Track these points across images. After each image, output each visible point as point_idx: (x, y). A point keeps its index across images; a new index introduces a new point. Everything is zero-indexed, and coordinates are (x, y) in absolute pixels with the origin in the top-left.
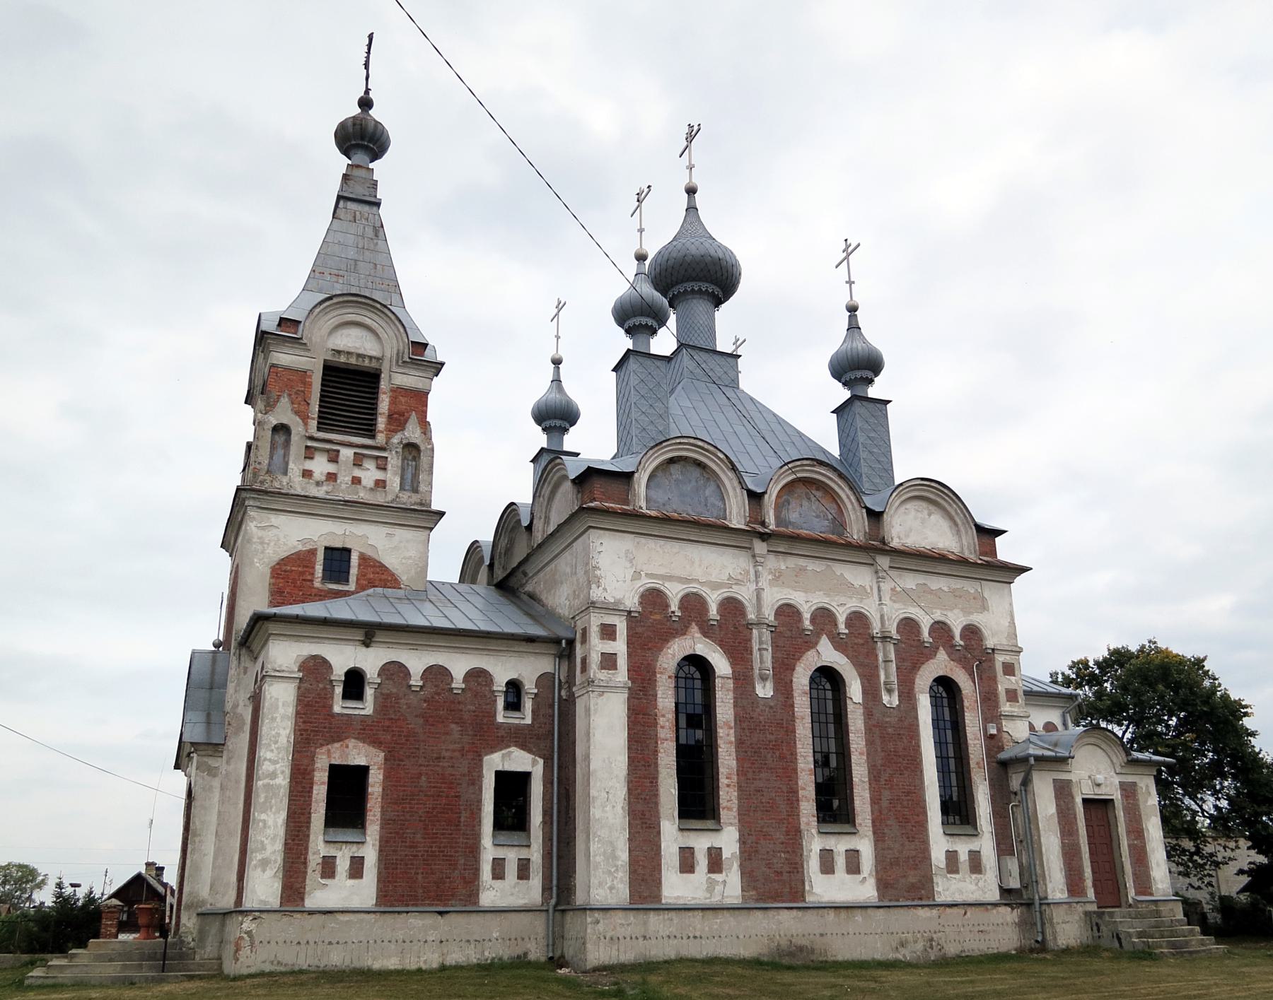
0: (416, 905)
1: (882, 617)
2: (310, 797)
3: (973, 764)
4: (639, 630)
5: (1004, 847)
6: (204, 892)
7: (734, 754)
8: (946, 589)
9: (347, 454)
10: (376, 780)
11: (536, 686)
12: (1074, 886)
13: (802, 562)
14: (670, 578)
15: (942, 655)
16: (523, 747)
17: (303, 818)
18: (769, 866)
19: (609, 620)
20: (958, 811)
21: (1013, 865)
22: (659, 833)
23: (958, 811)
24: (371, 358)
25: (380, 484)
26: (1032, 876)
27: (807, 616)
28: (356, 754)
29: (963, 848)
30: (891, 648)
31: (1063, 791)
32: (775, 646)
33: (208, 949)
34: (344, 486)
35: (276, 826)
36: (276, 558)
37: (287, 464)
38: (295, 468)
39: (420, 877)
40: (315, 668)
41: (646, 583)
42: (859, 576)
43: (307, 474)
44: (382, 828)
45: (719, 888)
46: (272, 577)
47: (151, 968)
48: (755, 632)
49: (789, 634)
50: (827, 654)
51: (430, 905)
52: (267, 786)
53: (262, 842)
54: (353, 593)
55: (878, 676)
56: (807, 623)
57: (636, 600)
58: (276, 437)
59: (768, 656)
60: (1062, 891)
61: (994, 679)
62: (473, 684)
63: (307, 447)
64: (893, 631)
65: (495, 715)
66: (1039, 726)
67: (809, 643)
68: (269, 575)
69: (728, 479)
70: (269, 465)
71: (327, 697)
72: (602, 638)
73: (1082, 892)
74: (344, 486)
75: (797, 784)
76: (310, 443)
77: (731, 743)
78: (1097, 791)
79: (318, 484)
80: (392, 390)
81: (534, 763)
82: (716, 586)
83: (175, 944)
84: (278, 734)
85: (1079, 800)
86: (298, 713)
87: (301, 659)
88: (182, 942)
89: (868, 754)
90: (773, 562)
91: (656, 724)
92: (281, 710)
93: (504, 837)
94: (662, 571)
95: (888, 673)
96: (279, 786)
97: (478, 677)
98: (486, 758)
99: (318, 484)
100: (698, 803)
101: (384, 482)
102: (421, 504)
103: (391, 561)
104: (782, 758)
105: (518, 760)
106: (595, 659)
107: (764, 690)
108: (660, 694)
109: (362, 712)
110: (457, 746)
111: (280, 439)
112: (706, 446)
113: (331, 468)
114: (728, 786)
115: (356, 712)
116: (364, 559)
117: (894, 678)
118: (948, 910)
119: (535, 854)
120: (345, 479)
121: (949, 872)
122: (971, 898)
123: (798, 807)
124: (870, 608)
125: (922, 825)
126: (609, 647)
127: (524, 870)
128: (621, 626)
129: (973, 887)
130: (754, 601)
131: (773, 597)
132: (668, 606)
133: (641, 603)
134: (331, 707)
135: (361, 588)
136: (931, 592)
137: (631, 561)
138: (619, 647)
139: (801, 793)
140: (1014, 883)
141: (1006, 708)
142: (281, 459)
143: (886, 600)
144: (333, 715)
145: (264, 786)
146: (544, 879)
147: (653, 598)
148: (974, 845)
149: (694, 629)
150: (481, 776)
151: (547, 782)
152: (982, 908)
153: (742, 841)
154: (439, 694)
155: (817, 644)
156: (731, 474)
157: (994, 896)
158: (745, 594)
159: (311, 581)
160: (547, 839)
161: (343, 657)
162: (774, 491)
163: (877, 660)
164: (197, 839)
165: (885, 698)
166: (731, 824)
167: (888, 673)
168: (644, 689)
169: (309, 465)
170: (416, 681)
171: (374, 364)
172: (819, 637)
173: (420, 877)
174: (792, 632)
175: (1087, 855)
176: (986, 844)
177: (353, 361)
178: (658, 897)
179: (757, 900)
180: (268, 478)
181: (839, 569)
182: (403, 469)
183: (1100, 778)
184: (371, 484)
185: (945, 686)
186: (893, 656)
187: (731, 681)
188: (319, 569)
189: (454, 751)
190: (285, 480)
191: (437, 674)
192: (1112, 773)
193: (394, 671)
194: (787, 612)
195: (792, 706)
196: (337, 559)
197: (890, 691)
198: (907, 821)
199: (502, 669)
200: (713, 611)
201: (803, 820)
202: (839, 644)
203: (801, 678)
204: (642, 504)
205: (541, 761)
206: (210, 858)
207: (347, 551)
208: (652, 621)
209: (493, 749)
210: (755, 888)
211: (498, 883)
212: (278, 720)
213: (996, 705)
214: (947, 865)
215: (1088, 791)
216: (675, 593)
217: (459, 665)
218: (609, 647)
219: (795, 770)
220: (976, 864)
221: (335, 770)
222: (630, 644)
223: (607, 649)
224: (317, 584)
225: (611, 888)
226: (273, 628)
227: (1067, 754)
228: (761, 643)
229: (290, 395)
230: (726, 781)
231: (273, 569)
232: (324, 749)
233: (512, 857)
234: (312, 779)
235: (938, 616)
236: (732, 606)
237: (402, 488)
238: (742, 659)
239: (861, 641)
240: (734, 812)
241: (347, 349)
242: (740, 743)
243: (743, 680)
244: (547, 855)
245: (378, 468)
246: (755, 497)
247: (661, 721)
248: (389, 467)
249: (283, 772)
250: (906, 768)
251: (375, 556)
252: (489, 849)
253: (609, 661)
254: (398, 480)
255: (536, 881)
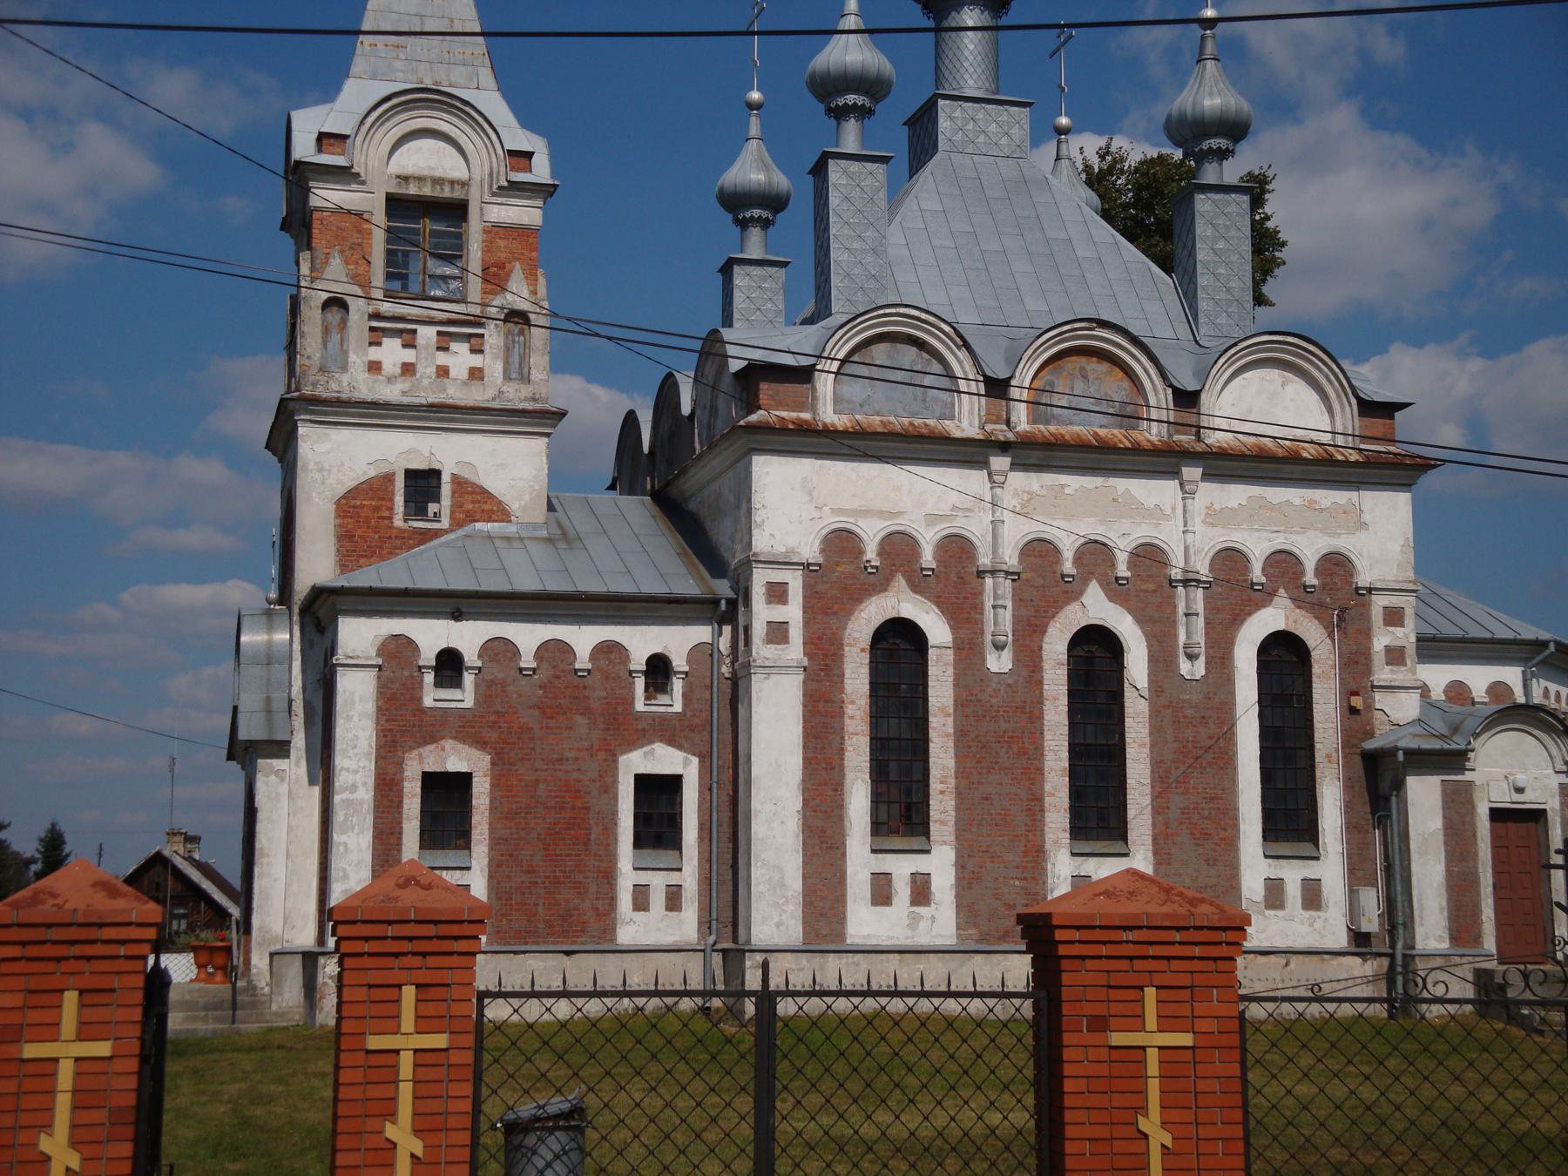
0: (537, 943)
1: (1186, 549)
2: (400, 813)
3: (1319, 756)
4: (819, 588)
5: (1357, 874)
6: (277, 926)
7: (951, 751)
8: (1297, 502)
9: (427, 334)
10: (481, 790)
11: (689, 662)
12: (1463, 928)
13: (1064, 479)
14: (866, 513)
15: (1282, 600)
16: (671, 742)
17: (392, 840)
18: (996, 897)
19: (778, 576)
20: (1290, 822)
21: (1371, 901)
22: (844, 855)
23: (1290, 822)
24: (452, 183)
25: (476, 374)
26: (1397, 913)
27: (1068, 555)
28: (455, 758)
29: (1293, 874)
30: (1199, 594)
31: (1457, 803)
32: (1018, 600)
33: (287, 996)
34: (425, 382)
35: (360, 850)
36: (341, 491)
37: (345, 354)
38: (357, 360)
39: (540, 909)
40: (398, 651)
41: (833, 522)
42: (1157, 492)
43: (375, 367)
44: (491, 849)
45: (923, 925)
46: (338, 516)
47: (218, 1020)
48: (989, 581)
49: (1039, 582)
50: (1097, 607)
51: (553, 943)
52: (348, 802)
53: (344, 870)
54: (446, 532)
55: (1176, 636)
56: (1068, 567)
57: (816, 546)
58: (329, 316)
59: (1007, 617)
60: (1440, 939)
61: (1366, 633)
62: (603, 663)
63: (372, 329)
64: (1202, 568)
65: (632, 702)
66: (1437, 693)
67: (1070, 591)
68: (333, 515)
69: (960, 363)
70: (323, 357)
71: (416, 687)
72: (769, 602)
73: (1477, 940)
74: (425, 382)
75: (1042, 788)
76: (375, 324)
77: (948, 735)
78: (1517, 797)
79: (390, 380)
80: (486, 232)
81: (686, 763)
82: (932, 519)
83: (245, 989)
84: (357, 737)
85: (1483, 811)
86: (379, 709)
87: (381, 640)
88: (255, 988)
89: (1152, 746)
90: (1018, 479)
91: (842, 713)
92: (359, 707)
93: (651, 856)
94: (855, 504)
95: (1192, 631)
96: (361, 802)
97: (609, 652)
98: (623, 759)
99: (390, 380)
100: (902, 815)
101: (481, 370)
102: (534, 399)
103: (495, 484)
104: (1023, 753)
105: (663, 759)
106: (759, 630)
107: (999, 663)
108: (848, 673)
109: (460, 705)
110: (586, 744)
111: (334, 316)
112: (924, 316)
113: (409, 356)
114: (942, 792)
115: (453, 705)
116: (457, 481)
117: (1200, 638)
118: (1261, 959)
119: (689, 877)
120: (426, 371)
121: (1268, 907)
122: (1300, 944)
123: (1042, 821)
124: (1170, 538)
125: (1230, 843)
126: (778, 613)
127: (674, 899)
128: (795, 582)
129: (1306, 928)
130: (990, 538)
131: (1015, 533)
132: (861, 552)
133: (822, 551)
134: (420, 699)
135: (457, 524)
136: (1271, 507)
137: (810, 493)
138: (793, 612)
139: (1048, 800)
140: (1371, 923)
141: (1383, 673)
142: (338, 347)
143: (1197, 524)
144: (423, 711)
145: (343, 801)
146: (701, 909)
147: (842, 542)
148: (1310, 870)
149: (900, 582)
150: (615, 782)
151: (706, 788)
152: (1316, 958)
153: (960, 865)
154: (558, 677)
155: (1081, 594)
156: (963, 354)
157: (1341, 940)
158: (976, 528)
159: (390, 518)
160: (706, 859)
161: (431, 635)
162: (1025, 375)
163: (1174, 611)
164: (264, 861)
165: (1185, 667)
166: (945, 843)
167: (1192, 631)
168: (827, 669)
169: (374, 354)
170: (528, 661)
171: (458, 194)
172: (1085, 582)
173: (540, 909)
174: (1043, 578)
175: (1490, 889)
176: (1331, 868)
177: (427, 191)
178: (840, 935)
179: (978, 941)
180: (323, 379)
181: (1122, 485)
182: (508, 350)
183: (1521, 779)
184: (465, 374)
185: (1283, 653)
186: (1199, 606)
187: (951, 652)
188: (399, 500)
189: (579, 750)
190: (345, 379)
191: (556, 652)
192: (1551, 771)
193: (499, 650)
194: (1039, 551)
195: (1040, 683)
196: (423, 484)
197: (1192, 657)
198: (1206, 835)
199: (641, 641)
200: (928, 558)
201: (1050, 837)
202: (1117, 590)
203: (1056, 645)
204: (828, 414)
205: (695, 760)
206: (281, 885)
207: (435, 474)
208: (839, 573)
209: (631, 745)
210: (976, 926)
211: (640, 916)
212: (356, 719)
213: (1368, 671)
214: (1266, 898)
215: (1503, 797)
216: (871, 534)
217: (583, 639)
218: (778, 613)
219: (1040, 771)
220: (1312, 896)
221: (431, 781)
222: (807, 608)
223: (775, 613)
224: (398, 521)
225: (778, 925)
226: (341, 602)
227: (1463, 747)
228: (996, 597)
229: (342, 252)
230: (940, 787)
231: (338, 503)
232: (414, 753)
233: (658, 882)
234: (401, 791)
235: (1279, 542)
236: (956, 548)
237: (507, 377)
238: (969, 621)
239: (1151, 587)
240: (950, 828)
241: (418, 173)
242: (961, 736)
243: (968, 650)
244: (706, 880)
245: (473, 351)
246: (997, 388)
247: (850, 710)
248: (487, 348)
249: (365, 784)
250: (1210, 764)
251: (476, 480)
252: (627, 875)
253: (778, 633)
254: (499, 366)
255: (690, 914)
